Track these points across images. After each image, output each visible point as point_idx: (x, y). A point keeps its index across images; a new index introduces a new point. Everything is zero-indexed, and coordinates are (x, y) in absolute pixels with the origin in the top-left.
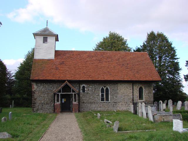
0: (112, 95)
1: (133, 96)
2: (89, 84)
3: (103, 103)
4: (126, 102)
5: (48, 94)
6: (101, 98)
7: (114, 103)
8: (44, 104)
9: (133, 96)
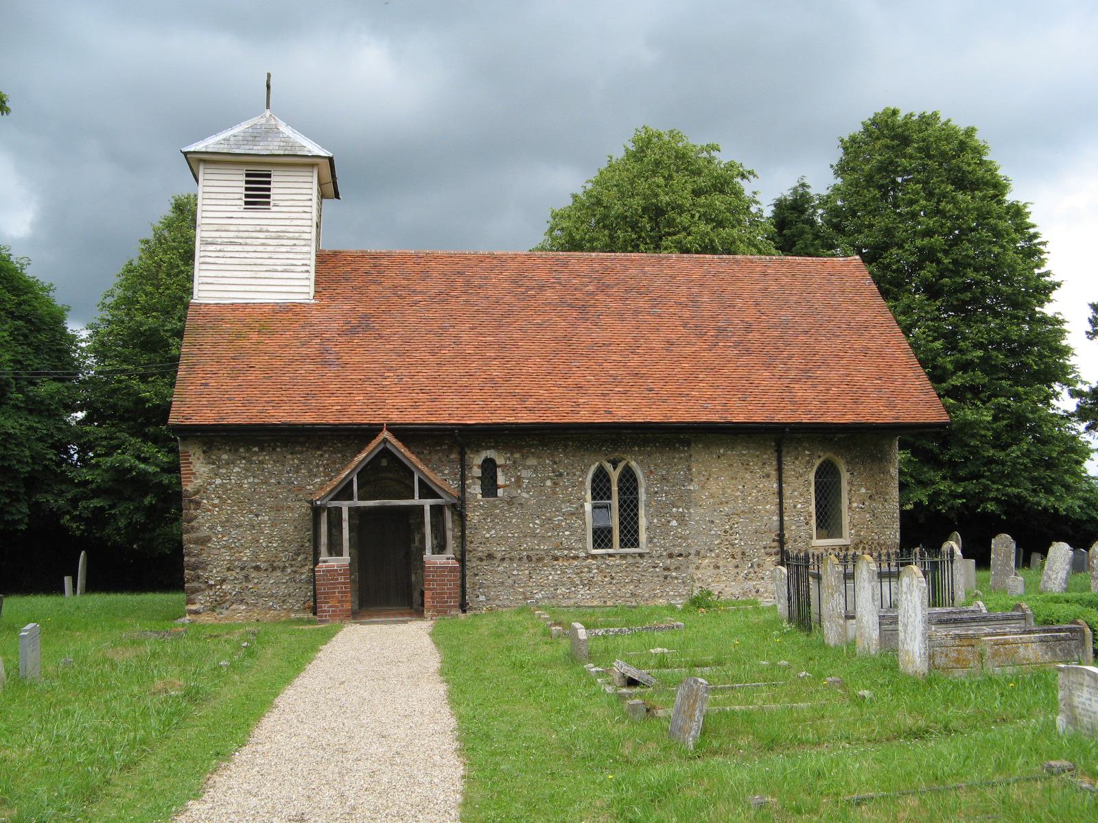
2: (519, 448)
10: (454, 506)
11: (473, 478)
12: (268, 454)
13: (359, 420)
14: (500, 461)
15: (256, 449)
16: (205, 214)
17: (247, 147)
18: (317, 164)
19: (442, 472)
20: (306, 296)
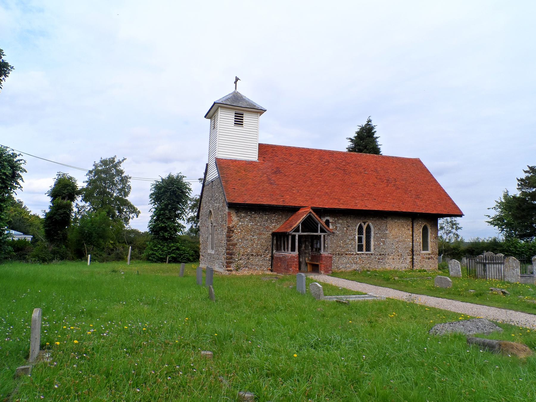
0: (377, 239)
1: (413, 243)
2: (336, 217)
3: (360, 254)
4: (400, 254)
5: (260, 234)
6: (358, 246)
7: (380, 255)
8: (252, 255)
9: (413, 243)
12: (257, 215)
15: (253, 213)
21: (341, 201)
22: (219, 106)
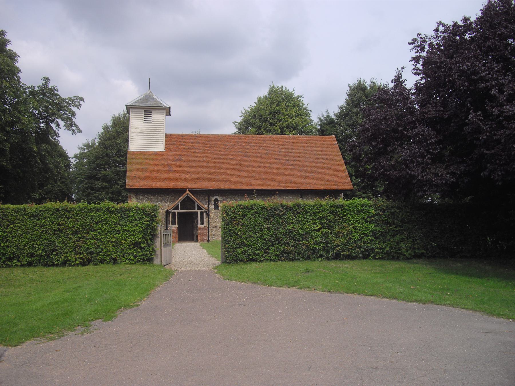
2: (225, 196)
10: (206, 212)
11: (212, 204)
12: (154, 197)
13: (180, 187)
14: (219, 199)
15: (150, 195)
16: (132, 124)
17: (144, 103)
18: (165, 109)
19: (203, 202)
20: (162, 149)
21: (228, 183)
22: (130, 107)
